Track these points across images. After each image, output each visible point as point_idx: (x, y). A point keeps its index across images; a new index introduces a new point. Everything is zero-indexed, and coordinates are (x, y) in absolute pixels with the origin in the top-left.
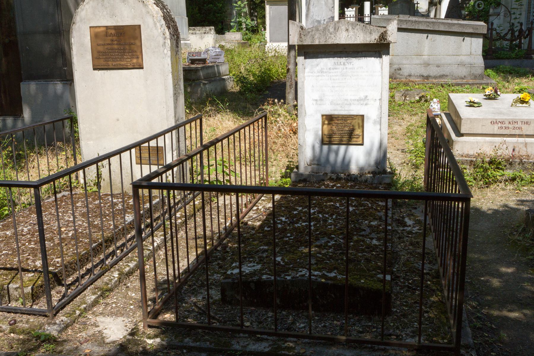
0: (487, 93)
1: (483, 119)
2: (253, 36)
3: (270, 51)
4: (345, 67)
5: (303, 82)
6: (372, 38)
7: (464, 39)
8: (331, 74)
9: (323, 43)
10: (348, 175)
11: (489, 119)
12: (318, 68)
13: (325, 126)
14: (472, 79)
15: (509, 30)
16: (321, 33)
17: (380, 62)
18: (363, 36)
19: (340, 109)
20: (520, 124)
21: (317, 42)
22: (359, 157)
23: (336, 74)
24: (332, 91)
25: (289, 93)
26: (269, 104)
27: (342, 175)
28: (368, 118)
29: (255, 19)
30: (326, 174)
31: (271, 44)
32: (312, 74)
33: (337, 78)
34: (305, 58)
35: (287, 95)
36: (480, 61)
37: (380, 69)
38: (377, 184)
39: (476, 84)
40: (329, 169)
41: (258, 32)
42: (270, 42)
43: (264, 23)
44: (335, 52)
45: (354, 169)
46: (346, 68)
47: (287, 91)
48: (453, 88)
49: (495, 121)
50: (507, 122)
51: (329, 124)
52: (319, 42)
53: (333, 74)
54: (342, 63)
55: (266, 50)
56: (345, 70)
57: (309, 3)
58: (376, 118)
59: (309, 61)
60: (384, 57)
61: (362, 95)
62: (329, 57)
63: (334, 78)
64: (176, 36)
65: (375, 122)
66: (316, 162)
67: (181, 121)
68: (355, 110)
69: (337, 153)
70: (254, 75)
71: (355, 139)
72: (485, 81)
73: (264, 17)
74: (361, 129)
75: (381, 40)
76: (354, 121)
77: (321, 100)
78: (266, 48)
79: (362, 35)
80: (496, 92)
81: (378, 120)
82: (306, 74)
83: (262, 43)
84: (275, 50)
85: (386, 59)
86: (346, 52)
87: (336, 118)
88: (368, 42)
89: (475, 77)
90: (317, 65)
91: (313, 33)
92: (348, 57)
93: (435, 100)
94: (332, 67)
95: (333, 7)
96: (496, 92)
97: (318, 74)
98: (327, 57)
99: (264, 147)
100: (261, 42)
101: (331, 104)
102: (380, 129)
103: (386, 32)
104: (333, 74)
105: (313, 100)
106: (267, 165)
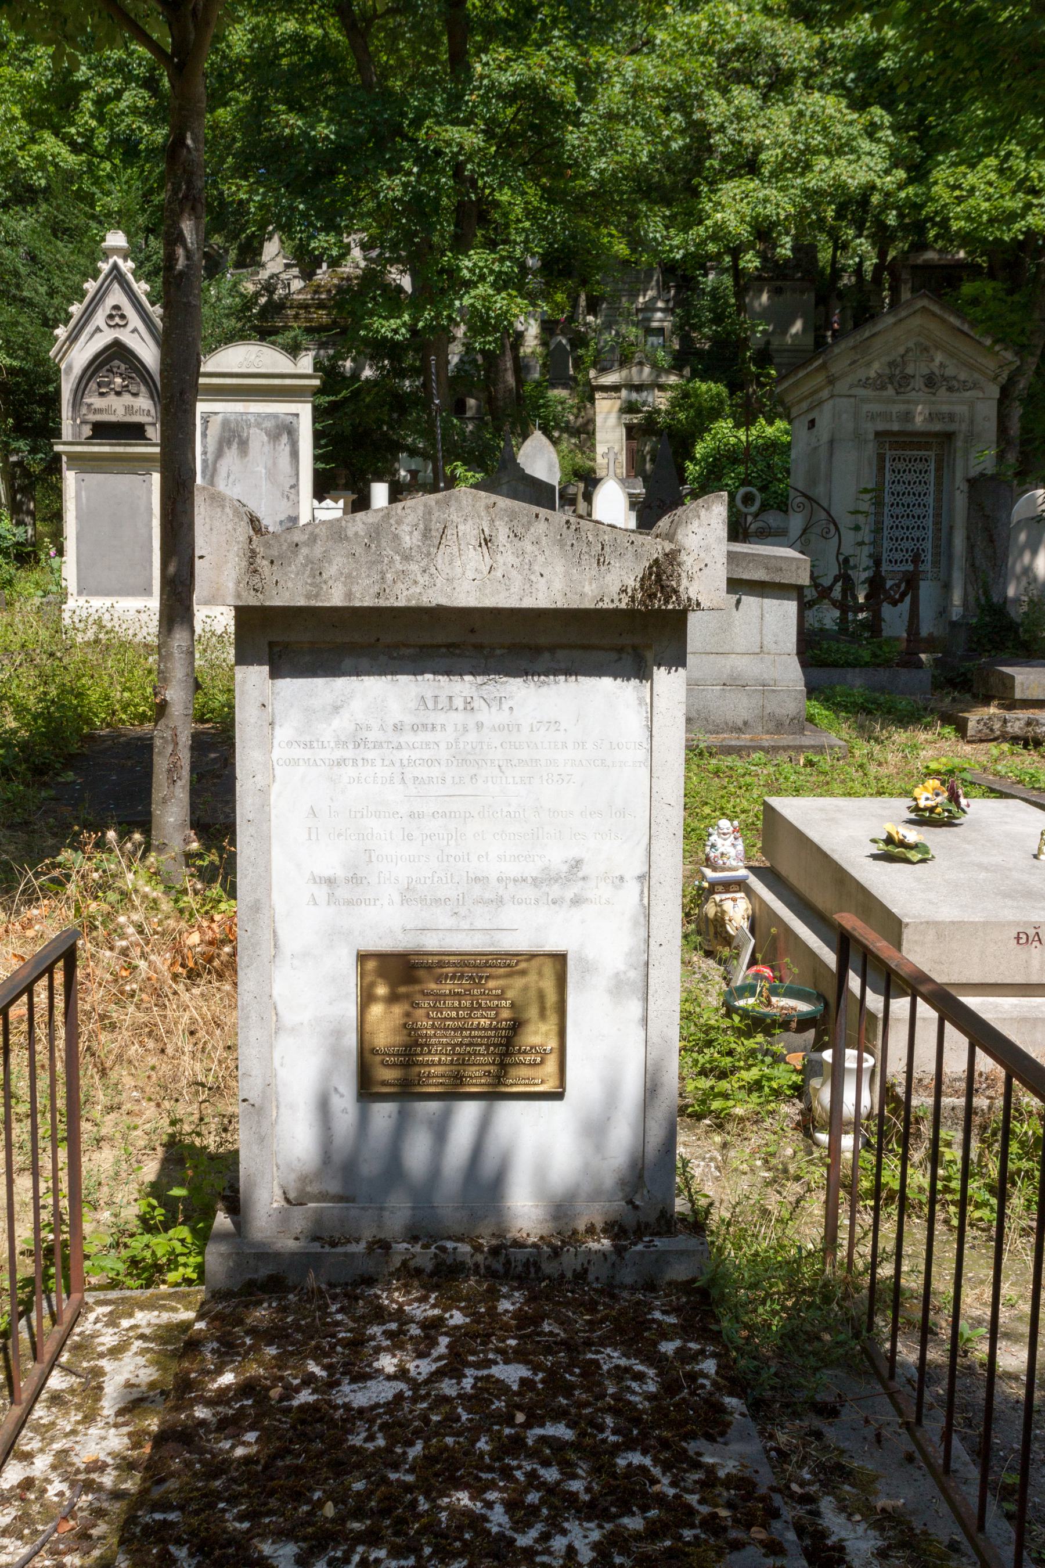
0: (922, 803)
1: (985, 924)
2: (21, 573)
3: (81, 626)
4: (471, 720)
5: (264, 792)
7: (738, 602)
8: (405, 754)
9: (368, 603)
10: (495, 1251)
11: (1010, 924)
12: (341, 723)
13: (377, 1010)
14: (768, 732)
15: (836, 580)
16: (359, 550)
17: (641, 701)
18: (567, 574)
19: (450, 922)
21: (335, 598)
22: (548, 1152)
23: (426, 754)
24: (410, 837)
25: (164, 801)
26: (78, 846)
27: (465, 1248)
28: (588, 968)
29: (28, 519)
30: (383, 1246)
31: (82, 601)
32: (307, 754)
33: (435, 771)
34: (274, 675)
35: (156, 810)
36: (790, 673)
37: (642, 735)
38: (633, 1289)
39: (786, 748)
40: (398, 1213)
41: (38, 561)
42: (80, 593)
43: (57, 536)
44: (422, 647)
45: (525, 1212)
46: (480, 726)
47: (157, 795)
48: (714, 761)
49: (1031, 932)
51: (393, 998)
52: (349, 595)
53: (415, 755)
54: (459, 702)
55: (67, 621)
56: (472, 736)
57: (215, 470)
58: (622, 967)
59: (290, 686)
60: (660, 674)
62: (394, 673)
63: (423, 772)
65: (618, 988)
66: (334, 1187)
68: (521, 929)
69: (441, 1132)
70: (20, 710)
71: (524, 1072)
72: (808, 739)
73: (58, 516)
74: (553, 1019)
75: (652, 596)
76: (519, 982)
77: (355, 880)
78: (66, 615)
79: (560, 569)
80: (954, 798)
81: (635, 975)
82: (276, 754)
83: (51, 597)
84: (99, 623)
85: (669, 684)
86: (479, 647)
87: (429, 967)
88: (588, 604)
89: (779, 726)
90: (336, 709)
91: (318, 550)
92: (485, 672)
93: (724, 823)
94: (409, 719)
95: (295, 486)
96: (954, 798)
97: (339, 754)
98: (382, 673)
99: (61, 1043)
100: (46, 593)
101: (404, 900)
102: (645, 1021)
103: (672, 557)
104: (415, 755)
105: (316, 880)
106: (73, 1139)
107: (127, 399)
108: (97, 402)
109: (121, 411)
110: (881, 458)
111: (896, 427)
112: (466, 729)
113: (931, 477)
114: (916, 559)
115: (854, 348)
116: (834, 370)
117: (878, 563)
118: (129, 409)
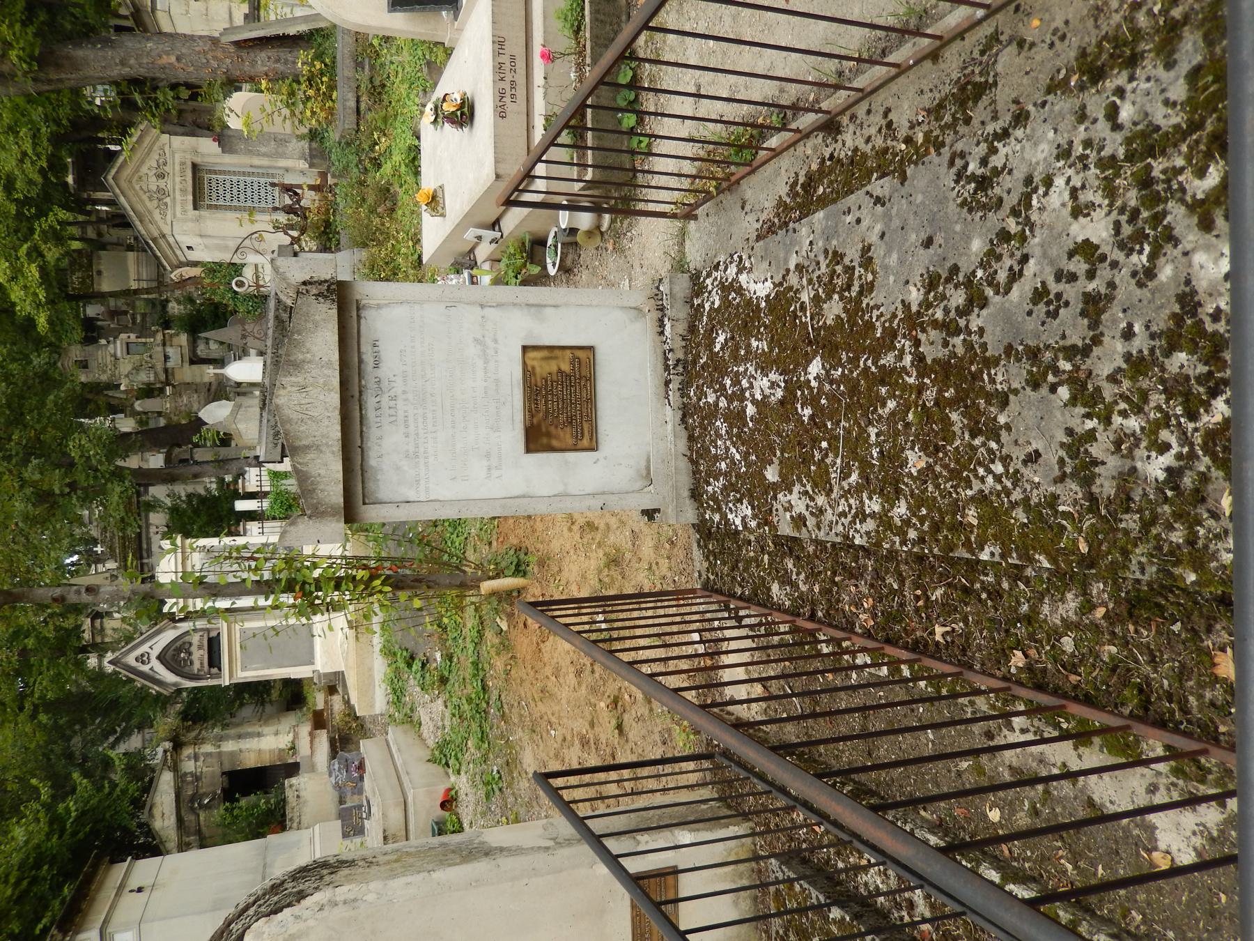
6: (326, 314)
8: (421, 432)
15: (286, 234)
20: (505, 59)
23: (420, 420)
32: (422, 482)
33: (430, 415)
46: (404, 392)
50: (501, 85)
56: (410, 396)
61: (472, 351)
64: (319, 872)
67: (565, 828)
77: (488, 455)
104: (421, 426)
107: (194, 649)
108: (197, 665)
109: (201, 652)
110: (210, 207)
111: (190, 198)
112: (406, 400)
113: (221, 177)
114: (273, 185)
115: (141, 221)
116: (156, 234)
117: (275, 209)
118: (200, 648)
